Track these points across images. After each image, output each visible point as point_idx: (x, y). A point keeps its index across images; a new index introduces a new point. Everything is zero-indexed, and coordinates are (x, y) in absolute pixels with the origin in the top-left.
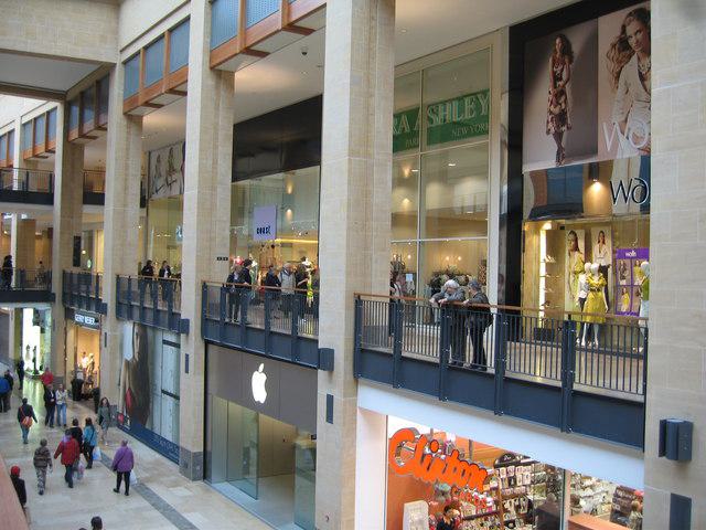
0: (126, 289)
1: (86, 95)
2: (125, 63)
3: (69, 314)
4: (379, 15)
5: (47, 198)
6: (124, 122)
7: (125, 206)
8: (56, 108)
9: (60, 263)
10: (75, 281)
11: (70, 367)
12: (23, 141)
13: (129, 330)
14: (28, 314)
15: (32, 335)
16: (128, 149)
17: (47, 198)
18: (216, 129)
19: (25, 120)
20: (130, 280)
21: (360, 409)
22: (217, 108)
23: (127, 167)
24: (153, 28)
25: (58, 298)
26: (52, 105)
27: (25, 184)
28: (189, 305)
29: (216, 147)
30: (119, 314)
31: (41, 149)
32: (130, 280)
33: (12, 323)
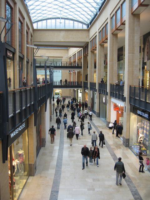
0: (133, 92)
1: (85, 47)
2: (91, 41)
3: (85, 90)
4: (114, 39)
5: (81, 67)
6: (91, 53)
7: (91, 69)
8: (81, 50)
9: (82, 79)
10: (137, 91)
11: (85, 101)
12: (99, 38)
13: (92, 92)
14: (79, 90)
15: (80, 95)
16: (92, 58)
17: (81, 67)
18: (101, 55)
19: (78, 51)
20: (135, 87)
21: (112, 102)
22: (101, 52)
23: (92, 61)
24: (100, 27)
25: (83, 87)
26: (81, 49)
27: (78, 64)
28: (97, 88)
29: (101, 59)
30: (111, 95)
31: (80, 58)
32: (135, 87)
33: (76, 91)
